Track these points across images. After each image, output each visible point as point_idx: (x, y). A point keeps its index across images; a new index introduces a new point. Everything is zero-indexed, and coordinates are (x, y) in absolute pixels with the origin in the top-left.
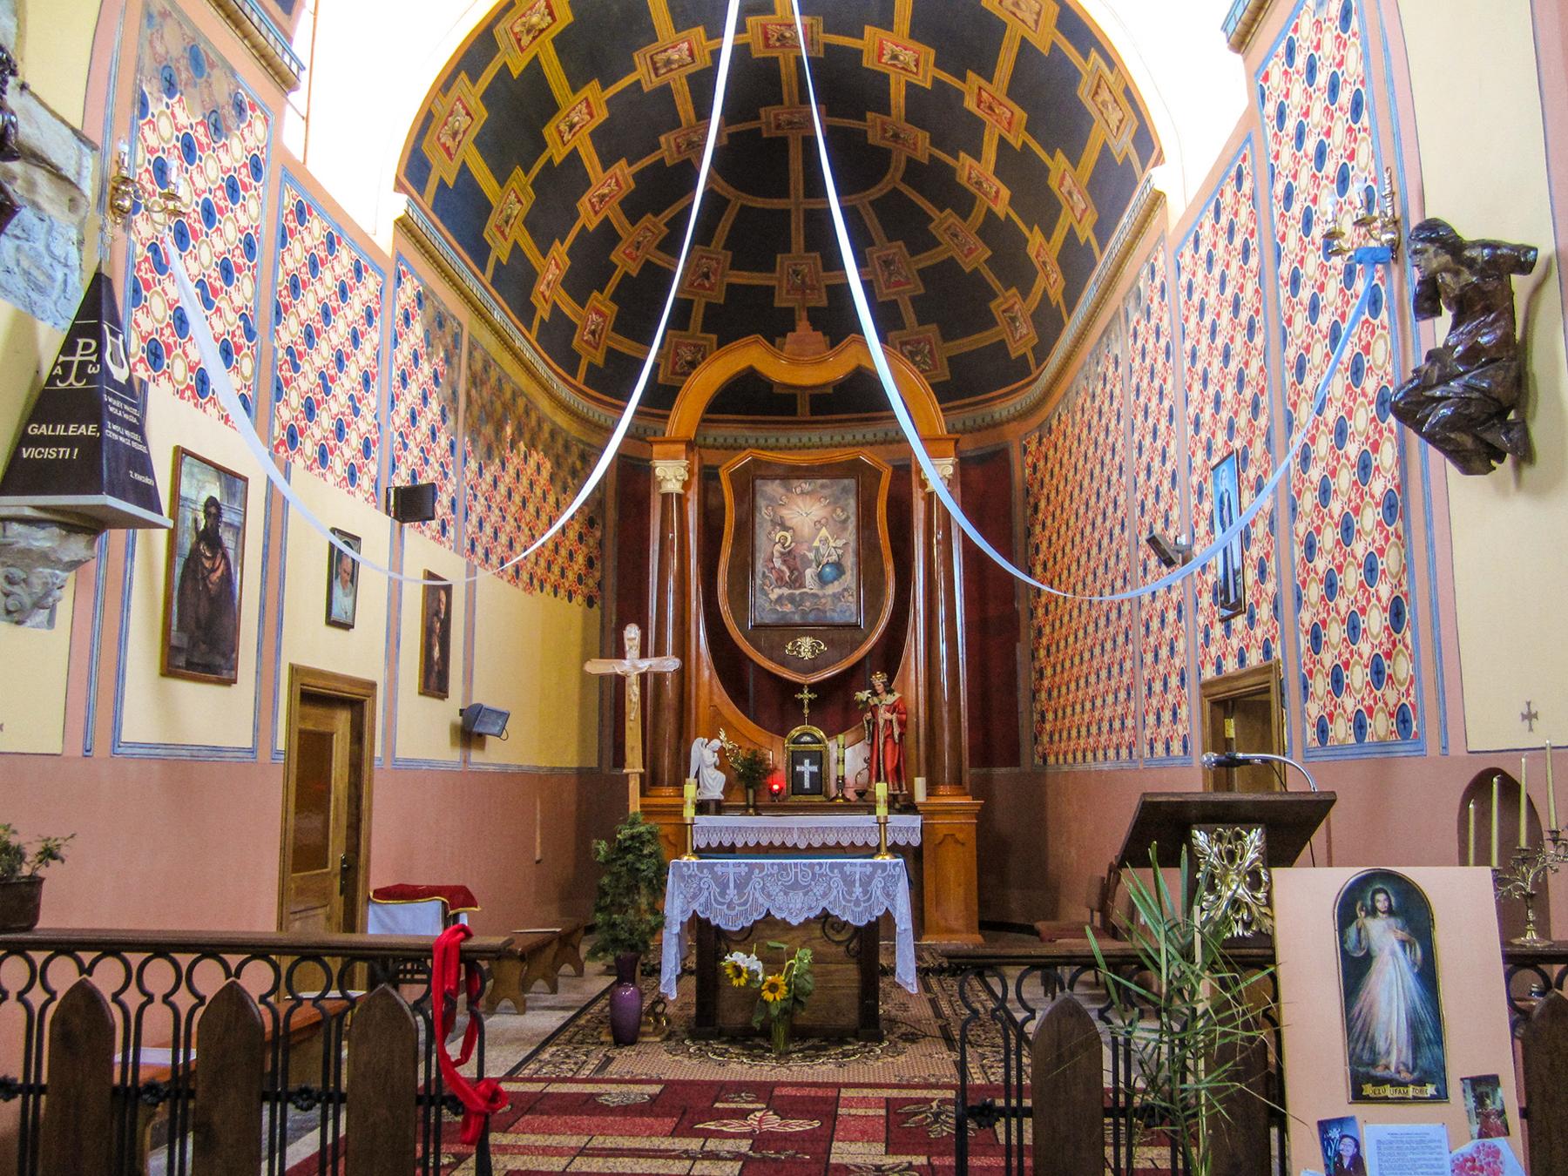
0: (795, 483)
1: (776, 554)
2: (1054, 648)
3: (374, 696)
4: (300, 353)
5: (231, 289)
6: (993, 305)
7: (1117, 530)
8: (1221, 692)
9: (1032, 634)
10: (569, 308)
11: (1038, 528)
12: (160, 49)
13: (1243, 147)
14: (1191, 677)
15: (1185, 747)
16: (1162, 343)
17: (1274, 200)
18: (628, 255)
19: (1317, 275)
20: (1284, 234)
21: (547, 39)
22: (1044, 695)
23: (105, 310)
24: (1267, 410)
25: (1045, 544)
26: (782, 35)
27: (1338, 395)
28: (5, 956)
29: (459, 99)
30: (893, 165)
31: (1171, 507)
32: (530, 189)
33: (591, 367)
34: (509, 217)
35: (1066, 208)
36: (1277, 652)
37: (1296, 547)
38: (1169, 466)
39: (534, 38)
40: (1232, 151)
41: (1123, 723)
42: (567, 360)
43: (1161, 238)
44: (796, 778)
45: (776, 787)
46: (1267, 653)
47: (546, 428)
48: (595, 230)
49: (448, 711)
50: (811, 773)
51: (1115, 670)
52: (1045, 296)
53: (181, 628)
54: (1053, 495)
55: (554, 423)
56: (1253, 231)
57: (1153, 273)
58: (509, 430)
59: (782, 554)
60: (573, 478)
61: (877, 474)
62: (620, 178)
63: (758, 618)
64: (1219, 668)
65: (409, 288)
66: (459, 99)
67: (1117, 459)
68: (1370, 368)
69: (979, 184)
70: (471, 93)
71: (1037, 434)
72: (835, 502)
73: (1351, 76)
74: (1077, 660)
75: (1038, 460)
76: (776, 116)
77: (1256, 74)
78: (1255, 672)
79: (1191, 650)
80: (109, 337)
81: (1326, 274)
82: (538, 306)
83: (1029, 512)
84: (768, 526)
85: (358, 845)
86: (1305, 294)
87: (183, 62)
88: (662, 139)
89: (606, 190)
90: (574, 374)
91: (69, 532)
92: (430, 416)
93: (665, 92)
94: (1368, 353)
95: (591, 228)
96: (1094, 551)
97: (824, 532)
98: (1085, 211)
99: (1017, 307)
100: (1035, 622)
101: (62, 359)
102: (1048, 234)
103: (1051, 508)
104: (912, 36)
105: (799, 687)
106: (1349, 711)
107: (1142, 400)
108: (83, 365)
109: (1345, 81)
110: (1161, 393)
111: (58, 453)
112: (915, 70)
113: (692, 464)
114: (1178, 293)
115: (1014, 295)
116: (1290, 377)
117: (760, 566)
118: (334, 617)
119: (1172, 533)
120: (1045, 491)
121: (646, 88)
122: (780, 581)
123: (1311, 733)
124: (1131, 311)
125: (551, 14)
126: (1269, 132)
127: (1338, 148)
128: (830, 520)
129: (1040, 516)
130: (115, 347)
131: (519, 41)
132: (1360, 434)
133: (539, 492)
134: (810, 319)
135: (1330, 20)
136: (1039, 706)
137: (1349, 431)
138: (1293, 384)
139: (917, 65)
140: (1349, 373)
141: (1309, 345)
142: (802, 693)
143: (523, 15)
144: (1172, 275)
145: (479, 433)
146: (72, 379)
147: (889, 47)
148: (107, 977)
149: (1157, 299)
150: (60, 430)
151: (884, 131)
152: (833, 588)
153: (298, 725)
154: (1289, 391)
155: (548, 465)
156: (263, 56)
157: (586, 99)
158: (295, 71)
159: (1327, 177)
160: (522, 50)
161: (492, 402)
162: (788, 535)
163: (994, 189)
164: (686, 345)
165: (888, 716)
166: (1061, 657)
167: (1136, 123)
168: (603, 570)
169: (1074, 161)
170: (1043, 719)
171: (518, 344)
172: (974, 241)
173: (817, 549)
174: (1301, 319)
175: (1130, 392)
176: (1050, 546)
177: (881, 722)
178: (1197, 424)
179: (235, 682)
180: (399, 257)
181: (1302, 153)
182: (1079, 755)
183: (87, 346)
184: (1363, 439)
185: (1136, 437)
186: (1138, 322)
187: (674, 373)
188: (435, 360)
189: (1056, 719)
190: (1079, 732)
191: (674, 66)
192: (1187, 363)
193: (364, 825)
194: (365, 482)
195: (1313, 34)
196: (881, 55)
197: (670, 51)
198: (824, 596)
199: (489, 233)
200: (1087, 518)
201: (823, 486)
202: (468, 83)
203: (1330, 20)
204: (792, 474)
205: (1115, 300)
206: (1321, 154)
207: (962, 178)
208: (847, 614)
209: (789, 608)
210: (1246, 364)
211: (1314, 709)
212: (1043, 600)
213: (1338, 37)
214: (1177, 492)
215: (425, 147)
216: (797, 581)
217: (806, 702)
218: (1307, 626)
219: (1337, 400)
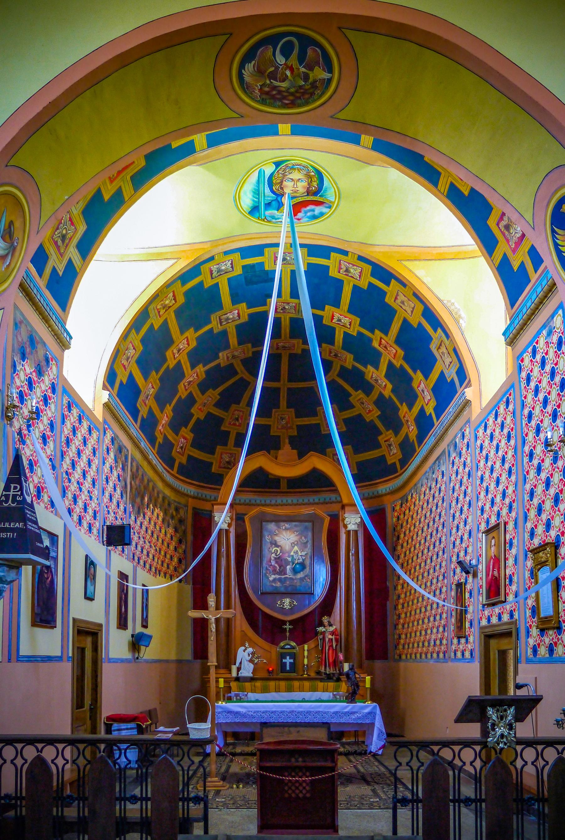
0: (282, 524)
1: (272, 558)
2: (406, 605)
3: (101, 630)
4: (70, 473)
5: (46, 447)
6: (380, 438)
7: (441, 553)
8: (489, 631)
9: (395, 598)
10: (171, 436)
11: (399, 548)
12: (20, 340)
13: (510, 389)
14: (475, 623)
15: (471, 654)
16: (467, 470)
17: (523, 417)
18: (200, 409)
19: (541, 455)
20: (527, 433)
21: (171, 311)
22: (400, 627)
23: (22, 472)
24: (516, 510)
25: (403, 555)
26: (284, 308)
27: (548, 509)
28: (3, 747)
29: (131, 342)
30: (333, 368)
31: (468, 546)
32: (158, 381)
33: (180, 464)
34: (148, 395)
35: (420, 398)
36: (516, 616)
37: (526, 572)
38: (468, 527)
39: (166, 311)
40: (504, 390)
41: (441, 642)
42: (169, 461)
43: (468, 421)
44: (283, 665)
45: (271, 669)
46: (512, 616)
47: (161, 496)
48: (185, 398)
49: (126, 635)
50: (290, 663)
51: (438, 618)
52: (407, 436)
53: (38, 605)
54: (407, 532)
55: (164, 493)
56: (513, 428)
57: (463, 436)
58: (146, 499)
59: (275, 558)
60: (172, 520)
61: (322, 520)
62: (199, 374)
63: (264, 589)
64: (489, 621)
65: (109, 435)
66: (131, 342)
67: (442, 520)
68: (562, 500)
69: (376, 380)
70: (136, 339)
71: (400, 502)
72: (301, 534)
73: (561, 371)
74: (418, 611)
75: (400, 514)
76: (277, 344)
77: (518, 357)
78: (506, 624)
79: (476, 611)
80: (24, 483)
81: (545, 455)
82: (158, 436)
83: (395, 539)
84: (269, 545)
85: (97, 697)
86: (535, 462)
87: (28, 343)
88: (220, 354)
89: (191, 379)
90: (172, 468)
91: (10, 568)
92: (117, 496)
93: (225, 333)
94: (561, 493)
95: (183, 397)
96: (429, 561)
97: (296, 548)
98: (430, 400)
99: (392, 439)
100: (397, 592)
101: (4, 493)
102: (410, 407)
103: (406, 538)
104: (349, 311)
105: (284, 622)
106: (547, 643)
107: (456, 494)
108: (14, 496)
109: (558, 372)
110: (465, 493)
111: (7, 535)
112: (349, 327)
113: (232, 515)
114: (476, 449)
115: (391, 434)
116: (527, 497)
117: (264, 564)
118: (88, 595)
119: (468, 558)
120: (403, 530)
121: (215, 331)
122: (275, 572)
123: (530, 651)
124: (452, 452)
125: (175, 299)
126: (523, 386)
127: (553, 401)
128: (299, 543)
129: (400, 541)
130: (26, 487)
131: (159, 312)
132: (556, 527)
133: (158, 528)
134: (291, 443)
135: (553, 343)
136: (398, 632)
137: (552, 525)
138: (528, 500)
139: (350, 325)
140: (553, 501)
141: (536, 485)
142: (286, 625)
143: (162, 301)
144: (473, 440)
145: (135, 502)
146: (10, 502)
147: (337, 315)
148: (49, 753)
149: (465, 449)
150: (7, 525)
151: (330, 352)
152: (300, 575)
153: (77, 645)
154: (526, 503)
155: (162, 514)
156: (56, 335)
157: (187, 337)
158: (68, 339)
159: (548, 413)
160: (160, 316)
161: (140, 486)
162: (279, 549)
163: (384, 384)
164: (226, 453)
165: (330, 637)
166: (410, 609)
167: (458, 365)
168: (186, 546)
169: (426, 377)
170: (400, 638)
171: (150, 457)
172: (371, 407)
173: (293, 556)
174: (532, 473)
175: (449, 490)
176: (405, 556)
177: (327, 640)
178: (482, 510)
179: (56, 627)
180: (105, 422)
181: (537, 399)
182: (418, 656)
183: (15, 488)
184: (558, 530)
185: (452, 511)
186: (455, 458)
187: (220, 467)
188: (119, 469)
189: (406, 638)
190: (418, 645)
191: (230, 321)
192: (478, 482)
193: (99, 688)
194: (95, 531)
195: (545, 347)
196: (332, 319)
197: (228, 314)
198: (296, 579)
199: (139, 404)
200: (425, 545)
201: (296, 526)
202: (135, 334)
203: (553, 343)
204: (278, 520)
205: (443, 445)
206: (545, 402)
207: (368, 377)
208: (307, 588)
209: (278, 584)
210: (507, 487)
211: (531, 642)
212: (401, 581)
213: (556, 352)
214: (471, 540)
215: (115, 366)
216: (283, 572)
217: (288, 629)
218: (530, 606)
219: (548, 511)
